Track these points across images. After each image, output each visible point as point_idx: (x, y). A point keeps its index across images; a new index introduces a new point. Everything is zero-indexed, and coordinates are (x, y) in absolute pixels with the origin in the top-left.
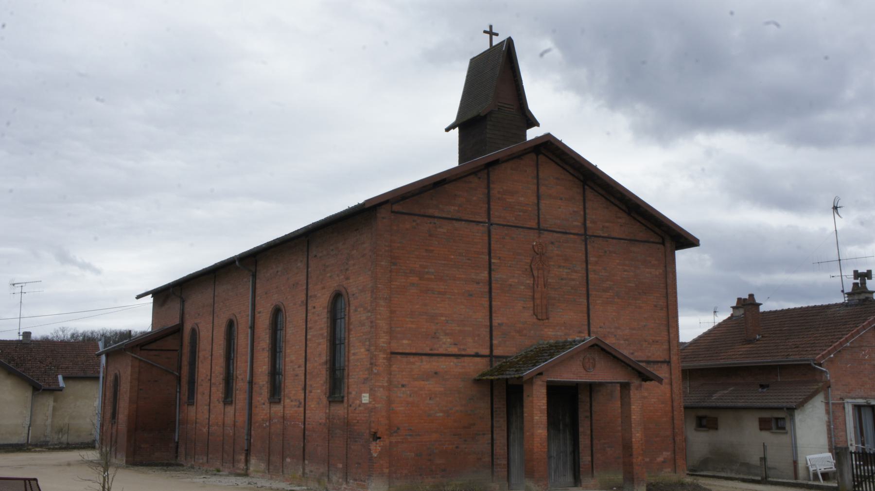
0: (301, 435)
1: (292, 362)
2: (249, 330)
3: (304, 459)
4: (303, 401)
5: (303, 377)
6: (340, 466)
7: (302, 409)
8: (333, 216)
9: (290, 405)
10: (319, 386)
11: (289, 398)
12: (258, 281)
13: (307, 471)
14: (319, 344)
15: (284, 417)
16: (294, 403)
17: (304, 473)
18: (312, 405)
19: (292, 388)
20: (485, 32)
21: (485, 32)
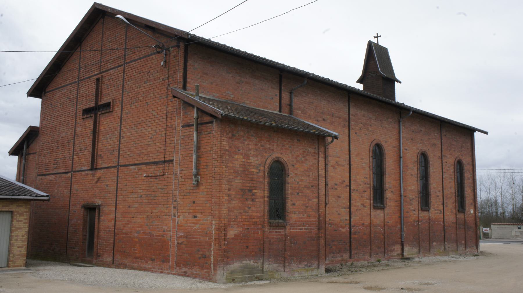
0: (442, 229)
1: (434, 188)
2: (402, 156)
3: (445, 242)
4: (442, 211)
5: (442, 198)
6: (463, 242)
7: (442, 215)
8: (448, 119)
9: (434, 212)
10: (451, 204)
11: (434, 208)
12: (383, 220)
13: (446, 247)
14: (450, 182)
15: (429, 219)
16: (437, 211)
17: (445, 249)
18: (447, 213)
19: (435, 201)
20: (377, 34)
21: (377, 34)
